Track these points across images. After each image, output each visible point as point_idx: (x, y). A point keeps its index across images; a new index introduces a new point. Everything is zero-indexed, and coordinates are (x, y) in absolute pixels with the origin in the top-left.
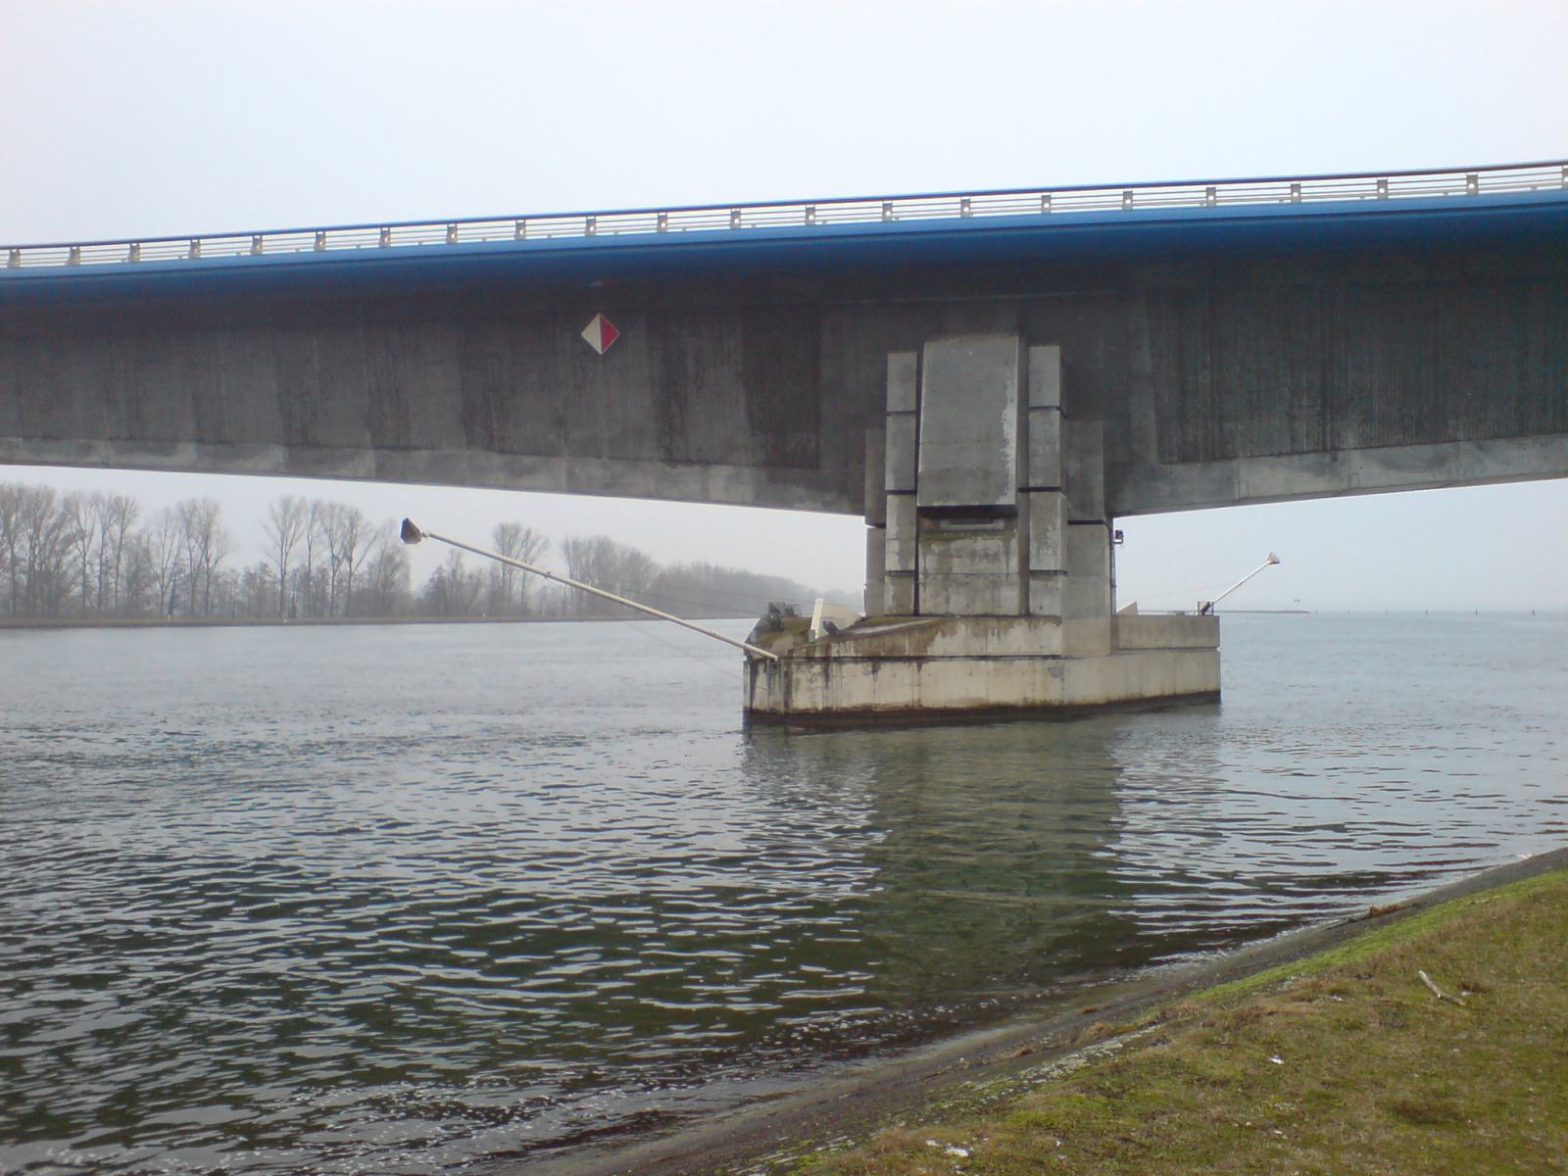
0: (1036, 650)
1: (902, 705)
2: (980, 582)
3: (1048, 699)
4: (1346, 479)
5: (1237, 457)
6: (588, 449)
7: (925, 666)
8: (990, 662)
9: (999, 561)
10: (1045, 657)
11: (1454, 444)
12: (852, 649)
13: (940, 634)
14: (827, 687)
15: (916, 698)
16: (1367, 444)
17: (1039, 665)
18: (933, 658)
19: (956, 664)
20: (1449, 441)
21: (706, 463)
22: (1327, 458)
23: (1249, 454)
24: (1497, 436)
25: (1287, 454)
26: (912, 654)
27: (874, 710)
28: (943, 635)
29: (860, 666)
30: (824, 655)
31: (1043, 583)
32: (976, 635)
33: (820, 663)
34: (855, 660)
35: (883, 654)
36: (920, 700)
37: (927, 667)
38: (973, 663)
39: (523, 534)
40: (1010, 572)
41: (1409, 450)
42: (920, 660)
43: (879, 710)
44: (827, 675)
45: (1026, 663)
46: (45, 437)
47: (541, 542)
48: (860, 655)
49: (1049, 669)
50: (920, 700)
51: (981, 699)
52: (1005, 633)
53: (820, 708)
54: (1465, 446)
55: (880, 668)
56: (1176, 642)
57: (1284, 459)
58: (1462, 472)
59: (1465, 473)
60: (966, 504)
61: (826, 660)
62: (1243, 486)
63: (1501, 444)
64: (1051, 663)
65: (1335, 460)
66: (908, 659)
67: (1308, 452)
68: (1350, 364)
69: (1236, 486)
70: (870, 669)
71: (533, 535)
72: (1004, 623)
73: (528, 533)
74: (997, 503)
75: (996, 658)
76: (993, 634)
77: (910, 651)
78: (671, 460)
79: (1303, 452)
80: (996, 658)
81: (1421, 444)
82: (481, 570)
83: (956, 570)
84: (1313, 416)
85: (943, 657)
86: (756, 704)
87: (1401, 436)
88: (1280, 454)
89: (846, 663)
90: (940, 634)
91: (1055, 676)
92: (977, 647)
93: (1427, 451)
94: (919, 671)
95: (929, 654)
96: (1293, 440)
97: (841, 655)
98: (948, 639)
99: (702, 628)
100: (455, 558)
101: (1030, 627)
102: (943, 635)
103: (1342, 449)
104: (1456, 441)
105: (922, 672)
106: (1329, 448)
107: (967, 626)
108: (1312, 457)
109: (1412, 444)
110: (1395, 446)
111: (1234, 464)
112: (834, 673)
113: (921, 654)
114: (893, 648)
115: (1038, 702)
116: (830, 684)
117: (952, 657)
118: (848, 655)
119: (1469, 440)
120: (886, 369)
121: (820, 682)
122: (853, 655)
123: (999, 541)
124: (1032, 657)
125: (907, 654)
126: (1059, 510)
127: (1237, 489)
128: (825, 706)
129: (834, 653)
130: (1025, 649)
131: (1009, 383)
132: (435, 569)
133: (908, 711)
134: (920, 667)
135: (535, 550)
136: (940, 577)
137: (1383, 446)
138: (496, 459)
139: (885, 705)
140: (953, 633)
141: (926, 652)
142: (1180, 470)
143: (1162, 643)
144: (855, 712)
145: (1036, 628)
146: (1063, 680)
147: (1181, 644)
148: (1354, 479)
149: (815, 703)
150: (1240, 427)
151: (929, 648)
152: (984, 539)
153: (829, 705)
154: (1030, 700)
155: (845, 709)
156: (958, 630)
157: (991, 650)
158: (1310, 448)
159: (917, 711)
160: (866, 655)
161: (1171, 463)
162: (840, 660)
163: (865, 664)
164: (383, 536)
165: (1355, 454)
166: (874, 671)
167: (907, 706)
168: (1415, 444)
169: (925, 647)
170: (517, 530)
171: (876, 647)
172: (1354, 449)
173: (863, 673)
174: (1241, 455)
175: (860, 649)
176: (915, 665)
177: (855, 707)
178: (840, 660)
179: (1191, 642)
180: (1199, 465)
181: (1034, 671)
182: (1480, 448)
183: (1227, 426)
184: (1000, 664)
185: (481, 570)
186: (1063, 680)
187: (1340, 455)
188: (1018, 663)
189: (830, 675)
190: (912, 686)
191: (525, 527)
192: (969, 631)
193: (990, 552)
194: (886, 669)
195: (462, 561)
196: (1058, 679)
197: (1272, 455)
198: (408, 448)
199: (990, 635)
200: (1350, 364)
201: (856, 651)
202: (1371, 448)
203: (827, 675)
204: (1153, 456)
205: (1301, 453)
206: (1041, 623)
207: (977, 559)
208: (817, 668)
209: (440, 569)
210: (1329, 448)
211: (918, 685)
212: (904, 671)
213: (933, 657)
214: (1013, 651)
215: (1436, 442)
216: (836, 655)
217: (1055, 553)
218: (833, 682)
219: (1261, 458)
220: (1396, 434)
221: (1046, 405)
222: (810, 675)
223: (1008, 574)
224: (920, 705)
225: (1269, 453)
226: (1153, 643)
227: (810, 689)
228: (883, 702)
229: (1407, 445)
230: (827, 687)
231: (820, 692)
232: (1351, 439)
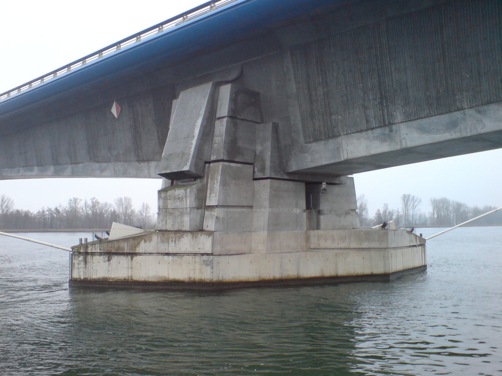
0: (196, 250)
1: (123, 279)
2: (177, 213)
3: (203, 278)
4: (399, 143)
5: (340, 135)
6: (117, 159)
7: (135, 258)
8: (170, 257)
9: (183, 201)
10: (203, 254)
11: (462, 111)
12: (98, 248)
13: (143, 241)
14: (85, 267)
15: (130, 275)
16: (408, 119)
17: (197, 258)
18: (140, 254)
19: (151, 257)
20: (458, 110)
21: (148, 161)
22: (387, 130)
23: (346, 133)
24: (489, 103)
25: (365, 130)
26: (128, 252)
27: (109, 280)
28: (145, 242)
29: (102, 257)
30: (85, 251)
31: (210, 212)
32: (162, 242)
33: (83, 255)
34: (101, 254)
35: (113, 251)
36: (132, 276)
37: (137, 259)
38: (160, 257)
39: (411, 198)
40: (187, 207)
41: (435, 119)
42: (133, 254)
43: (111, 280)
44: (86, 262)
45: (190, 258)
46: (12, 168)
47: (418, 200)
48: (102, 251)
49: (204, 261)
50: (132, 276)
51: (165, 276)
52: (179, 241)
53: (82, 278)
54: (471, 112)
55: (112, 259)
56: (354, 245)
57: (364, 134)
58: (468, 131)
59: (471, 131)
60: (172, 171)
61: (87, 253)
62: (345, 152)
63: (493, 107)
64: (205, 258)
65: (391, 131)
66: (127, 254)
67: (376, 128)
68: (393, 69)
69: (341, 152)
70: (107, 259)
71: (415, 198)
72: (178, 235)
73: (414, 197)
74: (182, 170)
75: (174, 254)
76: (172, 241)
77: (127, 250)
78: (139, 161)
79: (373, 128)
80: (174, 254)
81: (441, 114)
82: (393, 210)
83: (169, 207)
84: (377, 105)
85: (145, 253)
86: (76, 275)
87: (428, 111)
88: (361, 131)
89: (95, 255)
90: (143, 241)
91: (207, 265)
92: (163, 248)
93: (445, 118)
94: (132, 260)
95: (137, 251)
96: (367, 122)
97: (93, 251)
98: (148, 244)
99: (10, 237)
100: (386, 207)
101: (193, 237)
102: (145, 242)
103: (395, 124)
104: (463, 109)
105: (133, 261)
106: (387, 124)
107: (158, 237)
108: (378, 131)
109: (435, 115)
110: (425, 117)
111: (339, 139)
112: (89, 261)
113: (133, 252)
114: (118, 248)
115: (197, 280)
116: (87, 266)
117: (150, 253)
118: (96, 251)
119: (471, 107)
120: (217, 108)
121: (82, 264)
122: (99, 251)
123: (183, 190)
124: (195, 254)
125: (125, 251)
126: (220, 172)
127: (342, 154)
128: (84, 277)
129: (89, 251)
130: (190, 250)
131: (203, 106)
132: (377, 210)
133: (125, 282)
134: (132, 258)
135: (416, 203)
136: (164, 210)
137: (418, 119)
138: (96, 165)
139: (113, 278)
140: (150, 240)
141: (136, 250)
142: (314, 146)
143: (343, 245)
144: (99, 281)
145: (196, 238)
146: (212, 268)
147: (357, 246)
148: (404, 142)
149: (80, 275)
150: (340, 117)
151: (137, 249)
152: (179, 190)
153: (87, 277)
154: (192, 279)
155: (94, 279)
156: (153, 239)
157: (171, 250)
158: (377, 126)
159: (130, 282)
160: (105, 252)
161: (310, 142)
162: (93, 254)
163: (104, 256)
164: (360, 199)
165: (402, 126)
166: (109, 260)
167: (125, 279)
168: (437, 115)
169: (135, 247)
170: (409, 196)
171: (110, 247)
172: (401, 122)
173: (103, 261)
174: (342, 134)
175: (102, 248)
176: (129, 257)
177: (99, 279)
178: (93, 254)
179: (365, 245)
180: (323, 142)
181: (195, 262)
182: (479, 112)
183: (333, 117)
184: (176, 258)
185: (393, 210)
186: (212, 268)
187: (394, 127)
188: (186, 258)
189: (87, 261)
190: (128, 268)
191: (412, 195)
192: (159, 239)
193: (180, 197)
194: (115, 259)
195: (388, 207)
196: (209, 267)
197: (357, 132)
198: (78, 163)
199: (170, 241)
200: (393, 69)
201: (100, 249)
202: (411, 121)
203: (86, 262)
204: (302, 139)
205: (372, 129)
206: (200, 235)
207: (176, 200)
208: (81, 258)
209: (379, 210)
210: (387, 124)
211: (131, 268)
212: (124, 260)
213: (139, 253)
214: (183, 250)
215: (450, 112)
216: (91, 251)
217: (216, 195)
218: (89, 265)
219: (353, 135)
220: (424, 110)
221: (223, 116)
222: (78, 261)
223: (186, 208)
224: (132, 279)
225: (356, 131)
226: (335, 245)
227: (78, 268)
228: (113, 276)
229: (432, 116)
230: (85, 267)
231: (82, 270)
232: (399, 117)
